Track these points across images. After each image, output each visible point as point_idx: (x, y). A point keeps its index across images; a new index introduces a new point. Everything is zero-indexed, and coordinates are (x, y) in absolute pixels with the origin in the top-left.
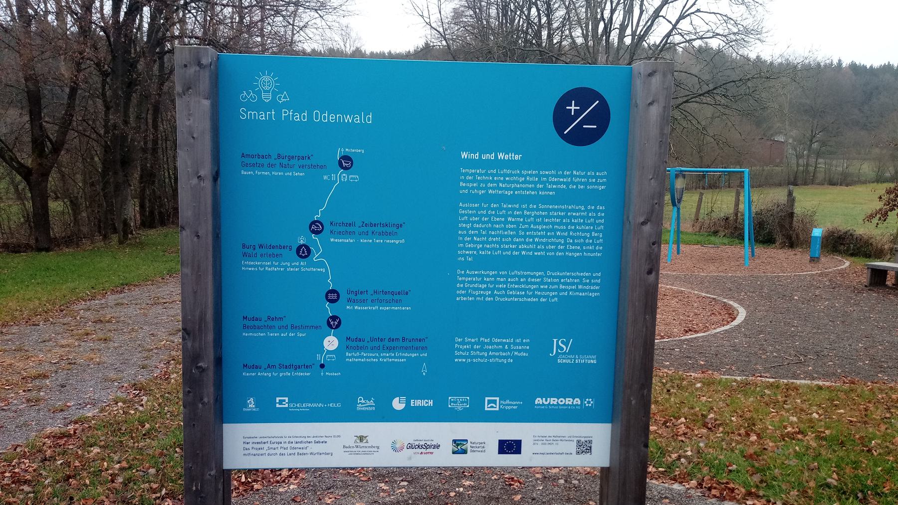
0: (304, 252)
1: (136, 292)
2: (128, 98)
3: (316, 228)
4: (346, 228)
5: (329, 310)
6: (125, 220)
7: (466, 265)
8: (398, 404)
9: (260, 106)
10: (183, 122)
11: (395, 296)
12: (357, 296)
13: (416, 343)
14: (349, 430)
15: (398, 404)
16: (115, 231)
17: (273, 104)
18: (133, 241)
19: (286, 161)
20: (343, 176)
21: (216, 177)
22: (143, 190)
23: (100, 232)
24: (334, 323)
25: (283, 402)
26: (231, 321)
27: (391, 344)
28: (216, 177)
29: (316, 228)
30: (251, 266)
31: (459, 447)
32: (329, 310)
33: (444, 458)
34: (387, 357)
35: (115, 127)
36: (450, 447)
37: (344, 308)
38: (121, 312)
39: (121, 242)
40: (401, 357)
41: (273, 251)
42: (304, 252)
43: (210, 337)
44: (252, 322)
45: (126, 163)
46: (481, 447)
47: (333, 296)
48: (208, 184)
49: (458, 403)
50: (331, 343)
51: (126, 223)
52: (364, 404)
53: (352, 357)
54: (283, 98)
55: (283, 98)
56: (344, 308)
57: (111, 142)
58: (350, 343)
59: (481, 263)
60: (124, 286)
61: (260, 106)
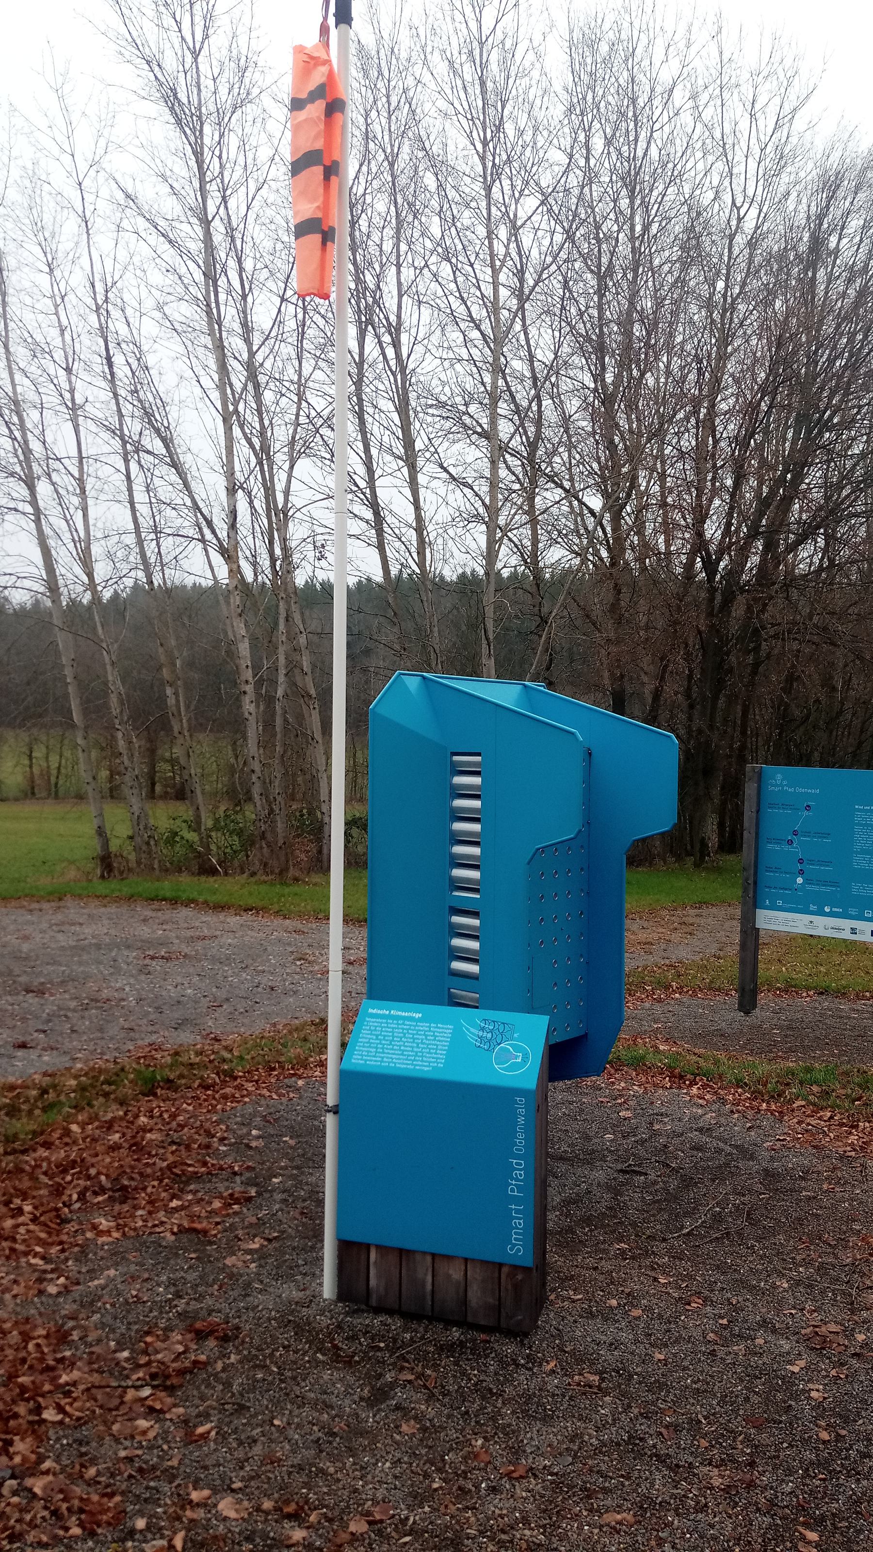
0: (790, 842)
1: (714, 910)
2: (716, 698)
3: (795, 833)
4: (807, 834)
5: (799, 867)
6: (703, 839)
7: (857, 853)
8: (827, 909)
9: (776, 785)
10: (747, 791)
11: (827, 863)
12: (811, 862)
13: (834, 884)
14: (808, 918)
15: (827, 909)
16: (689, 854)
17: (781, 785)
18: (709, 865)
19: (785, 806)
20: (806, 813)
21: (758, 811)
22: (724, 803)
23: (671, 852)
24: (801, 872)
25: (780, 903)
26: (761, 868)
27: (825, 884)
28: (758, 811)
29: (795, 833)
30: (770, 846)
31: (853, 931)
32: (799, 867)
33: (847, 935)
34: (823, 889)
35: (700, 731)
36: (849, 931)
37: (806, 867)
38: (702, 921)
39: (697, 865)
40: (829, 889)
41: (778, 841)
42: (790, 842)
43: (752, 872)
44: (769, 869)
45: (708, 772)
46: (862, 932)
47: (801, 861)
48: (754, 815)
49: (853, 912)
50: (800, 880)
51: (703, 844)
52: (813, 908)
53: (808, 887)
54: (785, 783)
55: (785, 783)
56: (806, 867)
57: (694, 748)
58: (807, 881)
59: (863, 852)
60: (701, 904)
61: (776, 785)
